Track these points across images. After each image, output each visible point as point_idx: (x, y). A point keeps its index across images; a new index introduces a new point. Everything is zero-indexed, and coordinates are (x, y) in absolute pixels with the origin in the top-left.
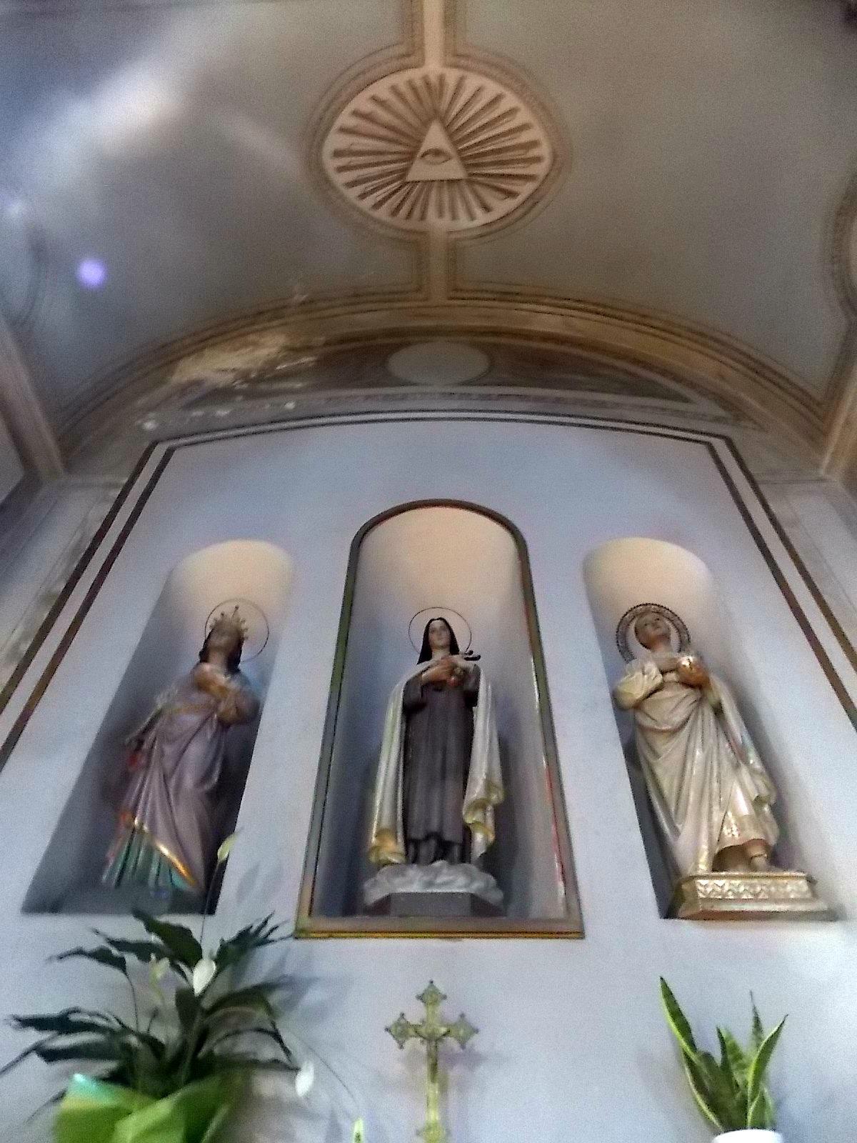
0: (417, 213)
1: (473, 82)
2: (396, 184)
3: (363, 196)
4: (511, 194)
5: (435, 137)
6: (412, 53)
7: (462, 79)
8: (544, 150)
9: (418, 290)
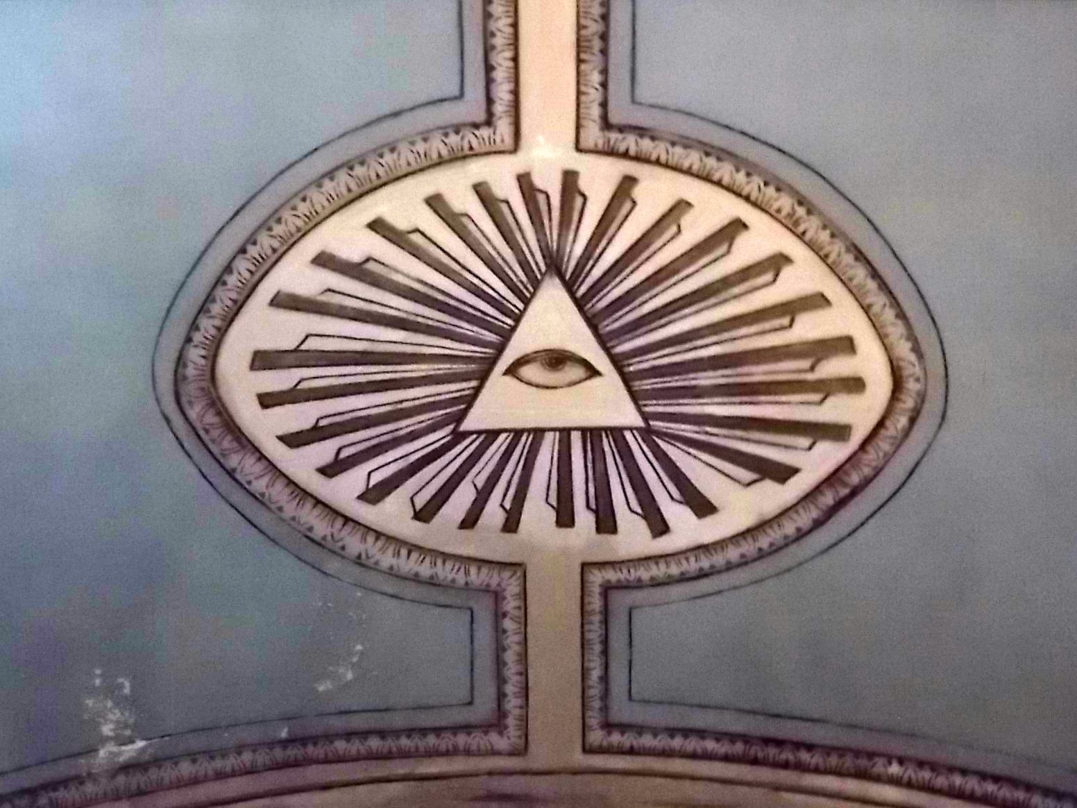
0: (493, 513)
1: (656, 191)
2: (442, 434)
3: (331, 470)
4: (783, 473)
5: (552, 320)
6: (496, 114)
7: (628, 182)
8: (870, 362)
9: (497, 723)
